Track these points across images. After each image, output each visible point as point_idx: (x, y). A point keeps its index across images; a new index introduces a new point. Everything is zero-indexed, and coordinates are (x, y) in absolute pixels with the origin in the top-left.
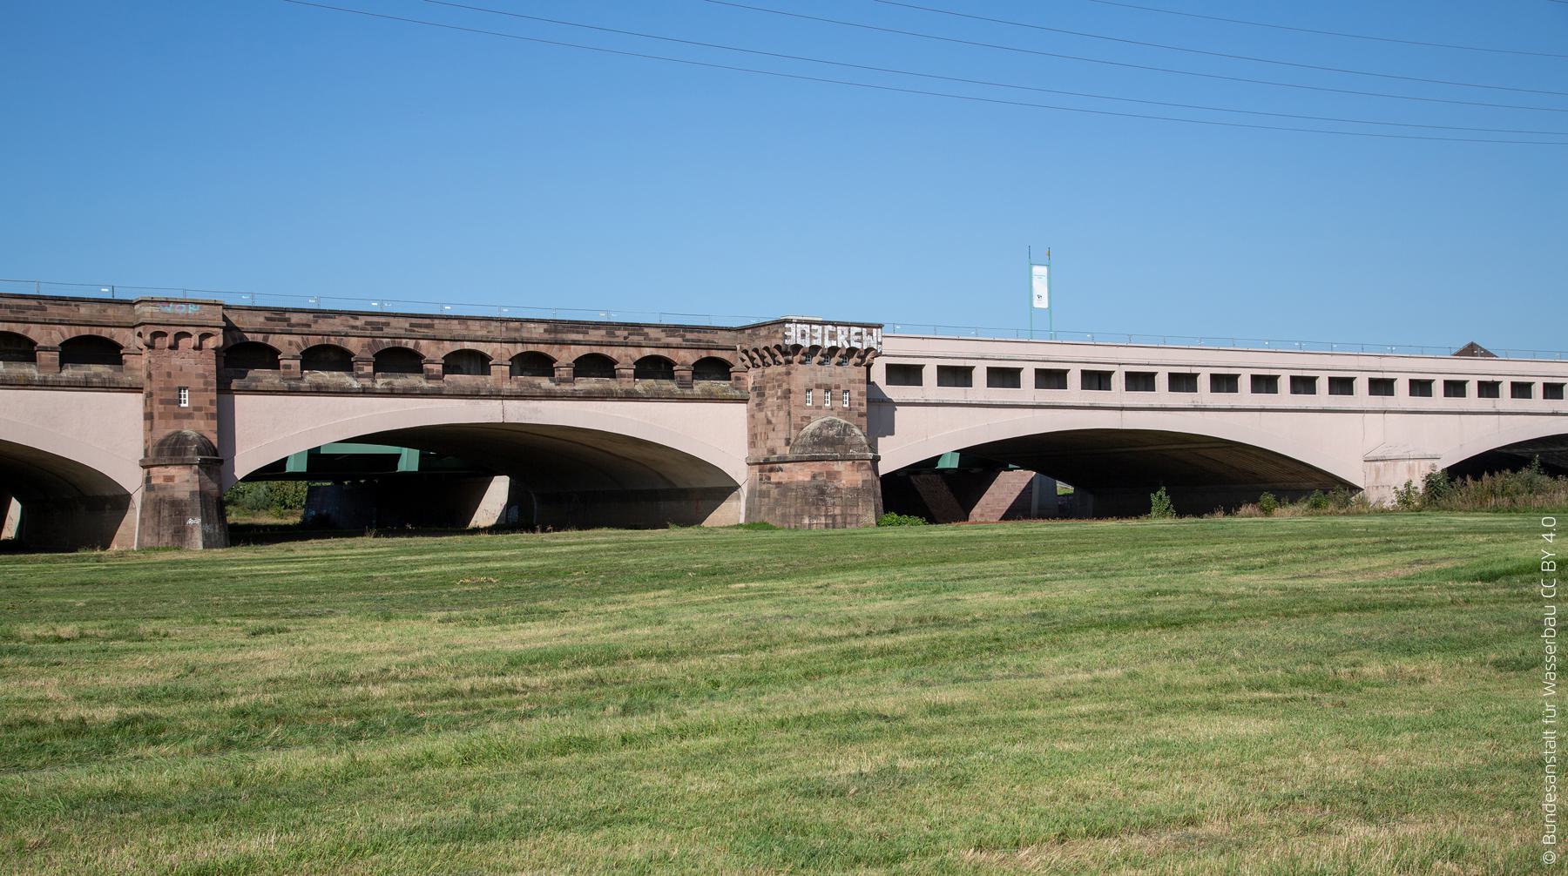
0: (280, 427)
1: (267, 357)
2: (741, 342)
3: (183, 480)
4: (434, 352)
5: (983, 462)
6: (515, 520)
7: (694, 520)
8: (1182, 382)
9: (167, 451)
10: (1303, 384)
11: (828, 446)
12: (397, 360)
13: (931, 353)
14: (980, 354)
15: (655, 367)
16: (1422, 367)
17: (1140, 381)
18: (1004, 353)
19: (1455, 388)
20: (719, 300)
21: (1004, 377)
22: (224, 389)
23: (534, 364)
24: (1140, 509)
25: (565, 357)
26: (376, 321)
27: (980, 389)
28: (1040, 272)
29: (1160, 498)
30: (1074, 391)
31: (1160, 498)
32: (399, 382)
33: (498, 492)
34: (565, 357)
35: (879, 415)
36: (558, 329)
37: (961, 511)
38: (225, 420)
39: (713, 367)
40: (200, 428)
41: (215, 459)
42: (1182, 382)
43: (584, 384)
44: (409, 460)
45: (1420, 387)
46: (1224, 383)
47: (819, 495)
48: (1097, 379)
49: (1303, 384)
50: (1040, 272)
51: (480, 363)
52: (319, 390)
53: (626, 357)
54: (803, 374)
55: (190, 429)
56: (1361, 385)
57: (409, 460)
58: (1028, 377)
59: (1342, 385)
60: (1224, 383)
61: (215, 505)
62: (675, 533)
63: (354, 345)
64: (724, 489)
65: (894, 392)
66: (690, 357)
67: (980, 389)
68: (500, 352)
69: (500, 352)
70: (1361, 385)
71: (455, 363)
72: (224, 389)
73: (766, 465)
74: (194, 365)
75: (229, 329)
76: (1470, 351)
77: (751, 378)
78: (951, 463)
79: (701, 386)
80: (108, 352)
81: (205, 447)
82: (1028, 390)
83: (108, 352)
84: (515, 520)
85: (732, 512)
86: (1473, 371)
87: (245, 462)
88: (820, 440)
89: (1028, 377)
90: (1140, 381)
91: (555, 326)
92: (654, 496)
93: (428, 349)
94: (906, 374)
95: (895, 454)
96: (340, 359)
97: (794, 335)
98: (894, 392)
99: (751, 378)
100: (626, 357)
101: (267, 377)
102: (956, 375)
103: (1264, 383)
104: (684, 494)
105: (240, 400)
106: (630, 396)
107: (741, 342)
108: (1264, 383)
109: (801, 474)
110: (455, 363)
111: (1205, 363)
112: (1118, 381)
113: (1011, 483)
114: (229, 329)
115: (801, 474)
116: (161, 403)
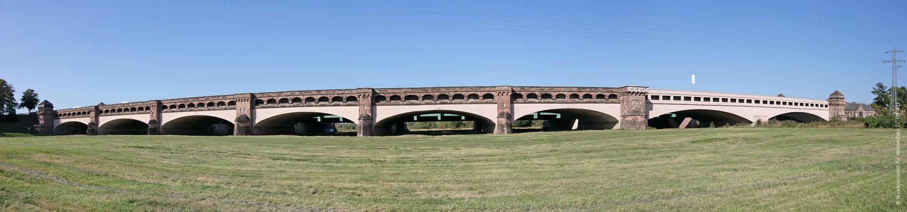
0: (384, 112)
1: (520, 96)
2: (619, 91)
3: (504, 121)
4: (554, 94)
5: (681, 115)
6: (580, 128)
7: (611, 128)
8: (716, 100)
9: (501, 115)
10: (741, 101)
11: (636, 113)
12: (546, 96)
13: (661, 93)
14: (672, 93)
15: (600, 96)
16: (772, 99)
17: (707, 99)
18: (688, 94)
19: (778, 103)
20: (614, 83)
21: (677, 98)
22: (512, 102)
23: (575, 96)
24: (708, 126)
25: (581, 94)
26: (542, 88)
27: (672, 100)
28: (693, 76)
29: (712, 124)
30: (692, 101)
31: (712, 124)
32: (546, 100)
33: (576, 125)
34: (581, 94)
35: (649, 106)
36: (580, 89)
37: (677, 127)
38: (373, 111)
39: (613, 96)
40: (508, 110)
41: (510, 116)
42: (716, 100)
43: (585, 100)
44: (559, 116)
45: (772, 103)
46: (725, 100)
47: (634, 123)
48: (697, 99)
49: (741, 101)
50: (693, 76)
51: (446, 97)
52: (530, 102)
53: (594, 94)
54: (631, 97)
55: (505, 111)
56: (753, 101)
57: (559, 116)
58: (682, 98)
59: (749, 101)
60: (725, 100)
61: (510, 126)
62: (606, 131)
63: (537, 93)
64: (616, 122)
65: (653, 101)
66: (608, 94)
67: (672, 100)
68: (567, 94)
69: (567, 94)
70: (753, 101)
71: (558, 96)
72: (512, 102)
73: (624, 117)
74: (507, 98)
75: (513, 91)
76: (780, 95)
77: (621, 98)
78: (674, 116)
79: (611, 100)
80: (491, 96)
81: (508, 114)
82: (682, 101)
83: (491, 96)
84: (580, 128)
85: (618, 126)
86: (781, 100)
87: (516, 117)
88: (635, 111)
89: (682, 98)
90: (697, 99)
91: (579, 88)
92: (603, 123)
93: (552, 93)
94: (656, 97)
95: (653, 115)
96: (534, 96)
97: (629, 89)
98: (653, 101)
99: (621, 98)
100: (594, 94)
101: (520, 100)
102: (666, 98)
103: (733, 100)
104: (609, 123)
105: (515, 105)
106: (595, 102)
107: (619, 91)
108: (733, 100)
109: (630, 119)
110: (558, 96)
111: (721, 96)
112: (702, 99)
113: (687, 120)
114: (513, 91)
115: (630, 119)
116: (501, 106)
